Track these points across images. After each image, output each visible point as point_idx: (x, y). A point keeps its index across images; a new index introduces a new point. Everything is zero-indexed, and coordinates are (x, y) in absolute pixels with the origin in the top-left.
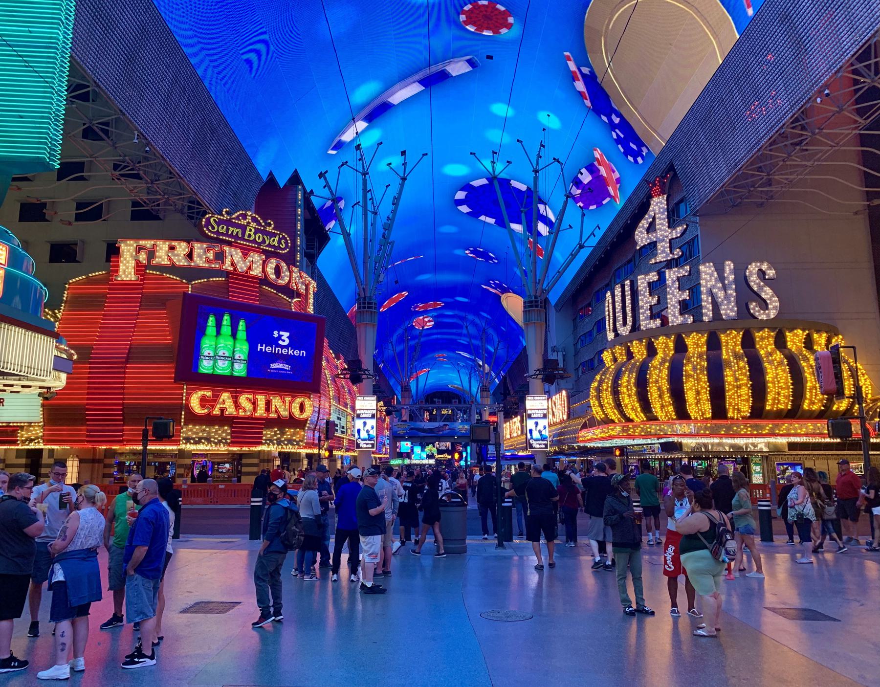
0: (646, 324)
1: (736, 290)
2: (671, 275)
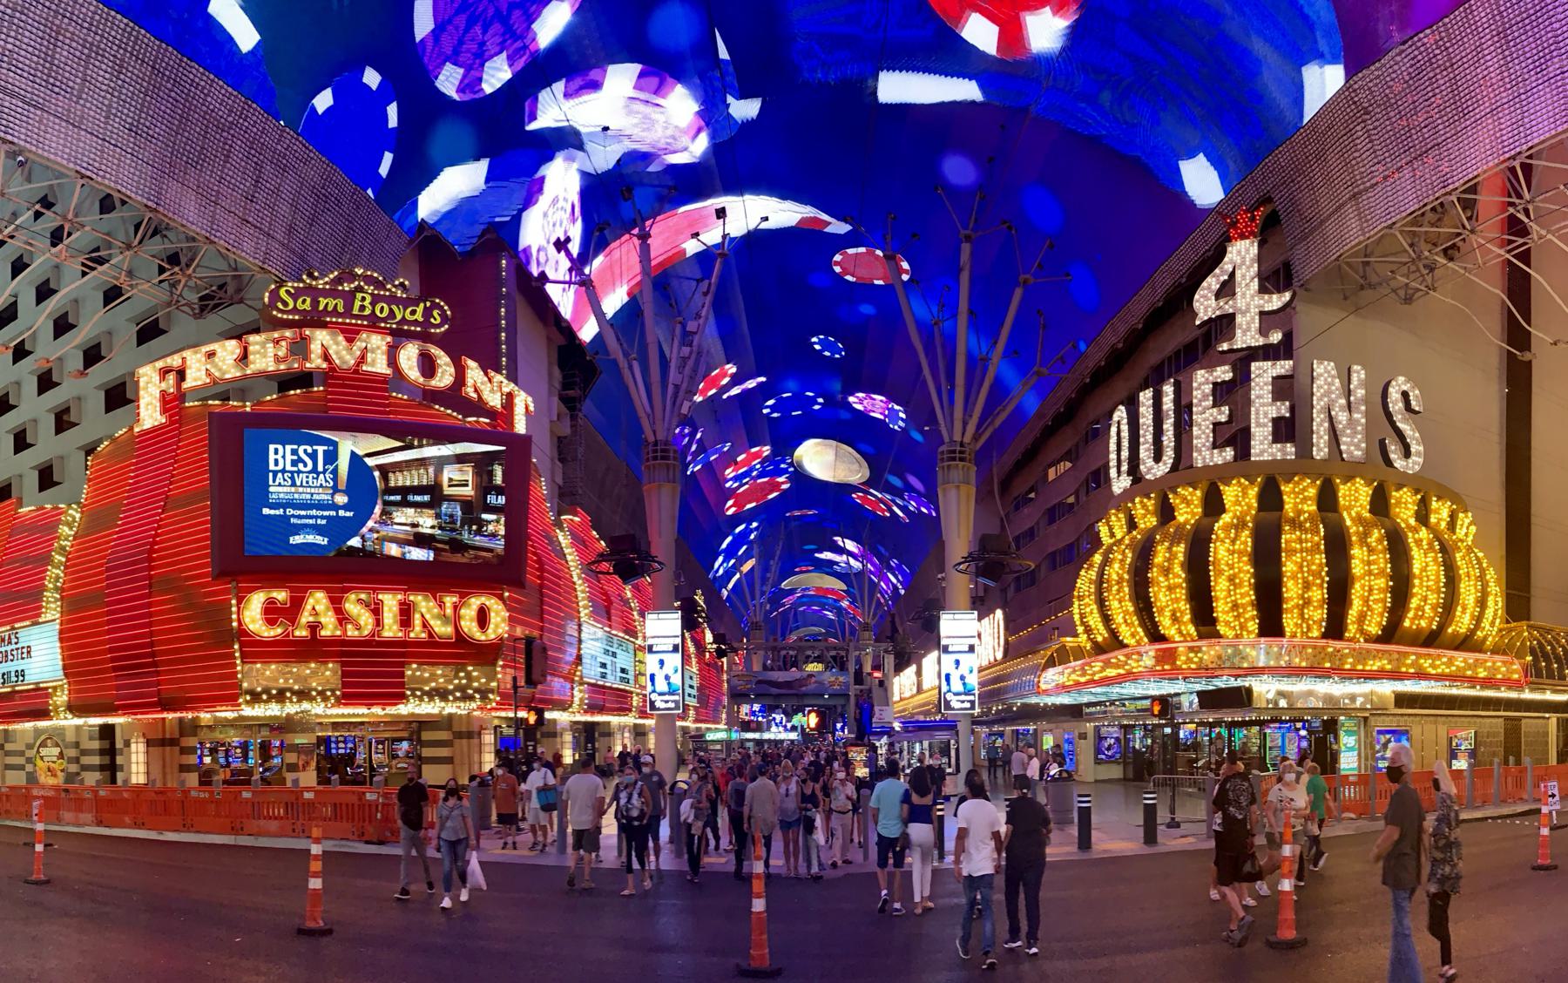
0: (1206, 455)
1: (1367, 414)
2: (1264, 373)
